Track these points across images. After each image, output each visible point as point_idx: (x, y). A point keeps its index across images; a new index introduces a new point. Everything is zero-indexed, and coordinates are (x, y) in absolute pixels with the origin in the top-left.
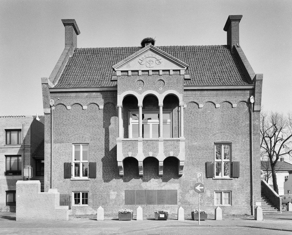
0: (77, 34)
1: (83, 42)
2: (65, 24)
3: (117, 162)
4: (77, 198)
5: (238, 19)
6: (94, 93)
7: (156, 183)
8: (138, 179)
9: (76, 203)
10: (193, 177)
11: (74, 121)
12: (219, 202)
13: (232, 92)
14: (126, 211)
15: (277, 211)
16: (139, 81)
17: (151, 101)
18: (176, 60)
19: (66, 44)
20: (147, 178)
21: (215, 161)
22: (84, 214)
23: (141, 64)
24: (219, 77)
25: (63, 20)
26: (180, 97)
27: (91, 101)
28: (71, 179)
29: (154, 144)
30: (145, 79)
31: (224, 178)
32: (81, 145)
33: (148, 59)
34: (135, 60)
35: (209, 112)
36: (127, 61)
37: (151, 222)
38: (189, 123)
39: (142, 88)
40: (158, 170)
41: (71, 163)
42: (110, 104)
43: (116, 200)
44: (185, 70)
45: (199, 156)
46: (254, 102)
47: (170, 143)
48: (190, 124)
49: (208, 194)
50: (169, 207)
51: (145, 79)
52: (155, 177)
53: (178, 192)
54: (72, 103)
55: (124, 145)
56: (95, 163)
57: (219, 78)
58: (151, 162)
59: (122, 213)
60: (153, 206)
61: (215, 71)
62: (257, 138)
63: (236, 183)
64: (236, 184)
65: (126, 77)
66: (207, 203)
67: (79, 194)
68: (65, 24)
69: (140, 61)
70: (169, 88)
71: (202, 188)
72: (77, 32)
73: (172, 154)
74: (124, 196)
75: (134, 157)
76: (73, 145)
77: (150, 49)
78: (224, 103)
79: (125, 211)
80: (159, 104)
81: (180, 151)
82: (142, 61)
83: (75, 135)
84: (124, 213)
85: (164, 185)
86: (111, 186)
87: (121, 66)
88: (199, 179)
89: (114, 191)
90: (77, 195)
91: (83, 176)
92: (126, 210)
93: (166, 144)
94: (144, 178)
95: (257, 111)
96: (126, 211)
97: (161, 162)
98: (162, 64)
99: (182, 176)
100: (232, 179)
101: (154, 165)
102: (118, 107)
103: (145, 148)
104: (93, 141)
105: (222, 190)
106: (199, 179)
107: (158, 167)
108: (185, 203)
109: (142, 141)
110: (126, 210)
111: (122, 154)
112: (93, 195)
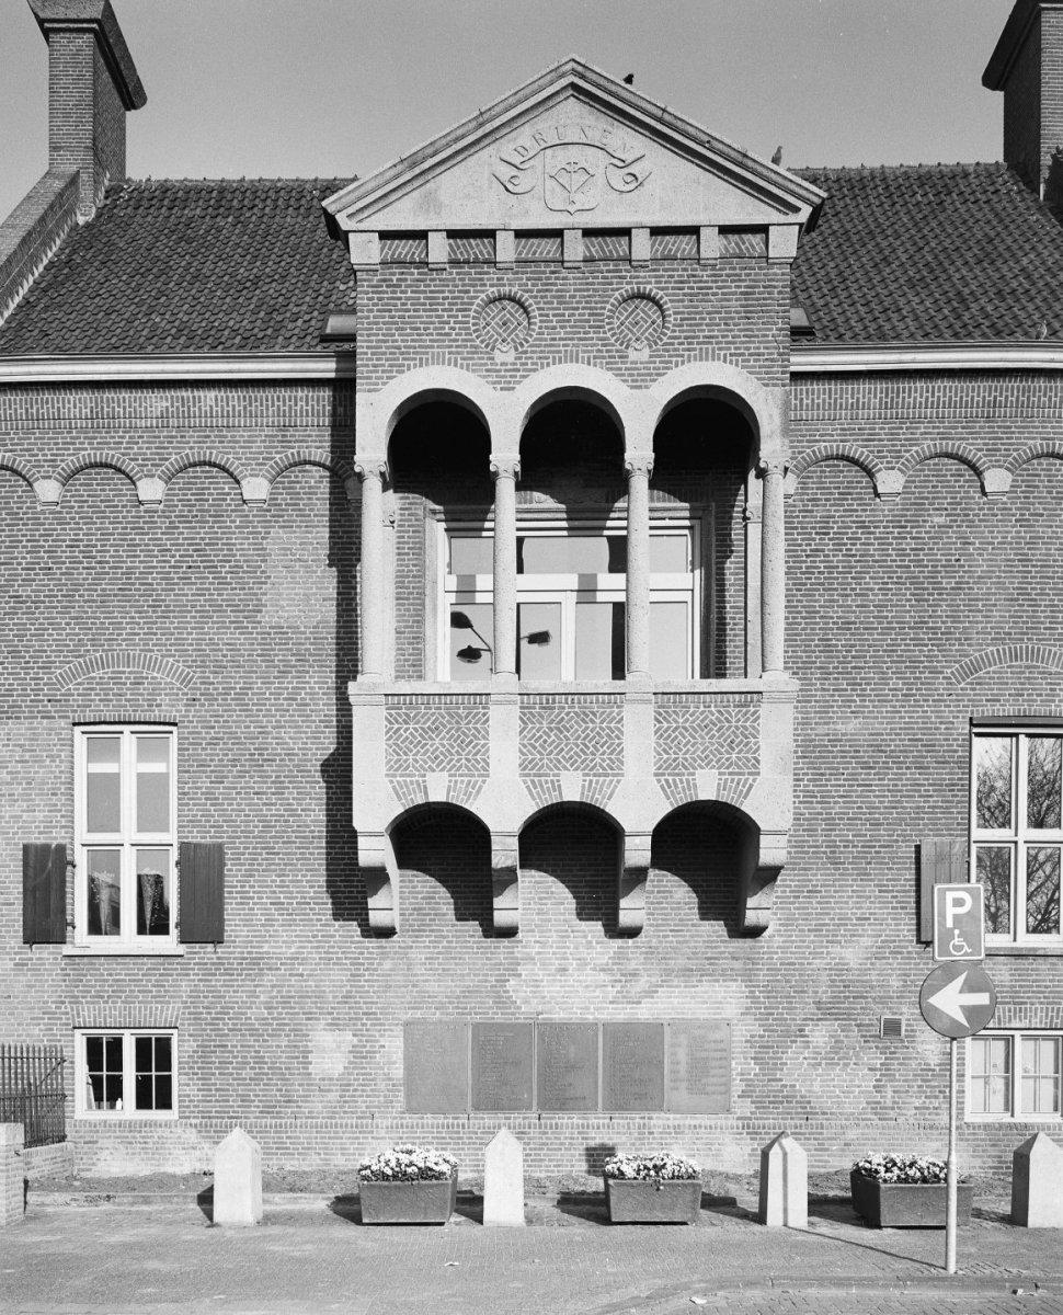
1: (160, 151)
3: (353, 835)
4: (154, 1073)
7: (602, 976)
10: (832, 942)
11: (81, 575)
12: (998, 1100)
14: (411, 1164)
16: (493, 301)
17: (573, 443)
18: (740, 158)
19: (54, 148)
21: (974, 837)
22: (145, 1170)
23: (510, 187)
24: (987, 316)
26: (766, 404)
27: (191, 448)
29: (592, 721)
30: (538, 291)
31: (1031, 949)
32: (127, 729)
33: (562, 157)
34: (472, 161)
35: (936, 519)
36: (417, 170)
37: (245, 897)
38: (809, 595)
39: (516, 349)
40: (616, 886)
41: (61, 849)
42: (307, 467)
43: (349, 1085)
44: (801, 225)
47: (696, 708)
48: (820, 599)
50: (678, 1130)
51: (538, 291)
52: (591, 942)
54: (70, 461)
55: (396, 726)
56: (220, 847)
57: (987, 324)
58: (574, 841)
59: (385, 1177)
60: (576, 1119)
61: (957, 289)
65: (413, 274)
66: (916, 1108)
67: (116, 1045)
68: (47, 25)
69: (506, 172)
70: (695, 347)
71: (982, 999)
72: (126, 86)
73: (707, 788)
75: (466, 806)
76: (78, 730)
78: (1035, 461)
79: (405, 1159)
80: (627, 456)
81: (763, 767)
82: (514, 172)
83: (90, 666)
84: (395, 1177)
85: (650, 993)
86: (320, 996)
87: (380, 198)
88: (957, 932)
89: (335, 1025)
90: (103, 1054)
91: (141, 930)
92: (410, 1152)
93: (668, 722)
94: (525, 947)
96: (411, 1164)
97: (637, 840)
98: (648, 186)
99: (766, 934)
101: (590, 865)
102: (360, 477)
103: (535, 748)
104: (204, 705)
106: (957, 932)
107: (616, 875)
108: (782, 1102)
110: (414, 1157)
111: (385, 787)
112: (204, 1052)
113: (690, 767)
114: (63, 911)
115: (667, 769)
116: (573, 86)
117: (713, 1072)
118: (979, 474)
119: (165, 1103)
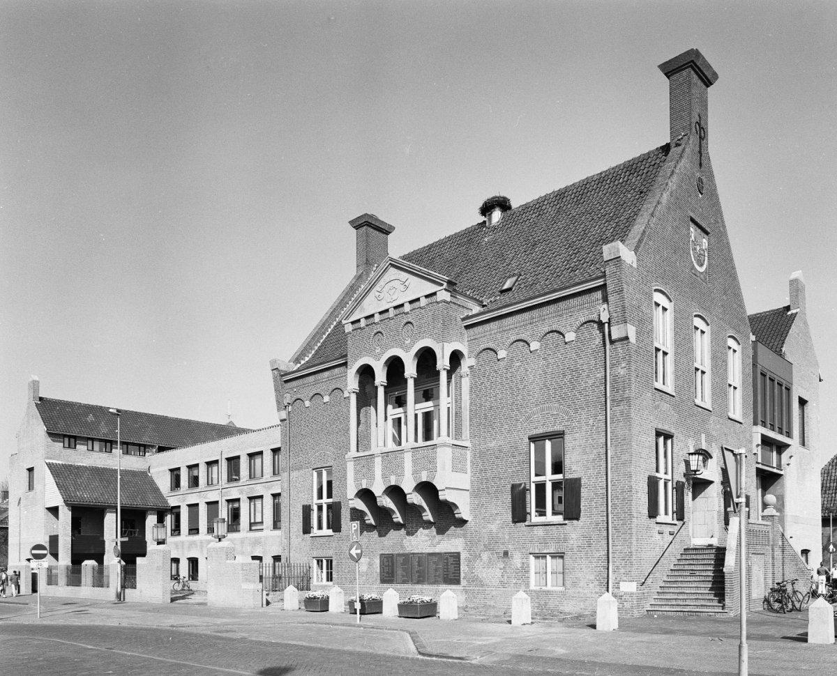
0: (708, 83)
2: (669, 72)
5: (687, 64)
6: (336, 370)
8: (398, 530)
9: (328, 580)
13: (562, 305)
15: (721, 608)
20: (412, 528)
21: (532, 480)
25: (351, 222)
28: (311, 535)
32: (323, 469)
41: (310, 506)
45: (499, 473)
46: (609, 319)
49: (517, 560)
53: (462, 557)
62: (622, 413)
63: (574, 531)
64: (574, 536)
69: (377, 294)
74: (378, 565)
76: (314, 471)
77: (390, 264)
82: (379, 294)
85: (439, 543)
95: (621, 340)
100: (566, 524)
105: (545, 552)
109: (379, 456)
113: (361, 479)
114: (310, 522)
115: (384, 476)
116: (390, 264)
117: (280, 573)
118: (529, 345)
119: (331, 580)
